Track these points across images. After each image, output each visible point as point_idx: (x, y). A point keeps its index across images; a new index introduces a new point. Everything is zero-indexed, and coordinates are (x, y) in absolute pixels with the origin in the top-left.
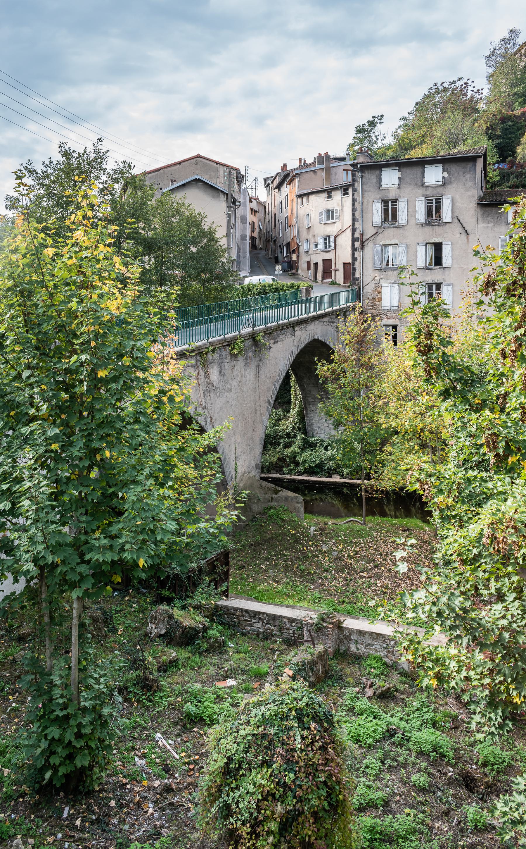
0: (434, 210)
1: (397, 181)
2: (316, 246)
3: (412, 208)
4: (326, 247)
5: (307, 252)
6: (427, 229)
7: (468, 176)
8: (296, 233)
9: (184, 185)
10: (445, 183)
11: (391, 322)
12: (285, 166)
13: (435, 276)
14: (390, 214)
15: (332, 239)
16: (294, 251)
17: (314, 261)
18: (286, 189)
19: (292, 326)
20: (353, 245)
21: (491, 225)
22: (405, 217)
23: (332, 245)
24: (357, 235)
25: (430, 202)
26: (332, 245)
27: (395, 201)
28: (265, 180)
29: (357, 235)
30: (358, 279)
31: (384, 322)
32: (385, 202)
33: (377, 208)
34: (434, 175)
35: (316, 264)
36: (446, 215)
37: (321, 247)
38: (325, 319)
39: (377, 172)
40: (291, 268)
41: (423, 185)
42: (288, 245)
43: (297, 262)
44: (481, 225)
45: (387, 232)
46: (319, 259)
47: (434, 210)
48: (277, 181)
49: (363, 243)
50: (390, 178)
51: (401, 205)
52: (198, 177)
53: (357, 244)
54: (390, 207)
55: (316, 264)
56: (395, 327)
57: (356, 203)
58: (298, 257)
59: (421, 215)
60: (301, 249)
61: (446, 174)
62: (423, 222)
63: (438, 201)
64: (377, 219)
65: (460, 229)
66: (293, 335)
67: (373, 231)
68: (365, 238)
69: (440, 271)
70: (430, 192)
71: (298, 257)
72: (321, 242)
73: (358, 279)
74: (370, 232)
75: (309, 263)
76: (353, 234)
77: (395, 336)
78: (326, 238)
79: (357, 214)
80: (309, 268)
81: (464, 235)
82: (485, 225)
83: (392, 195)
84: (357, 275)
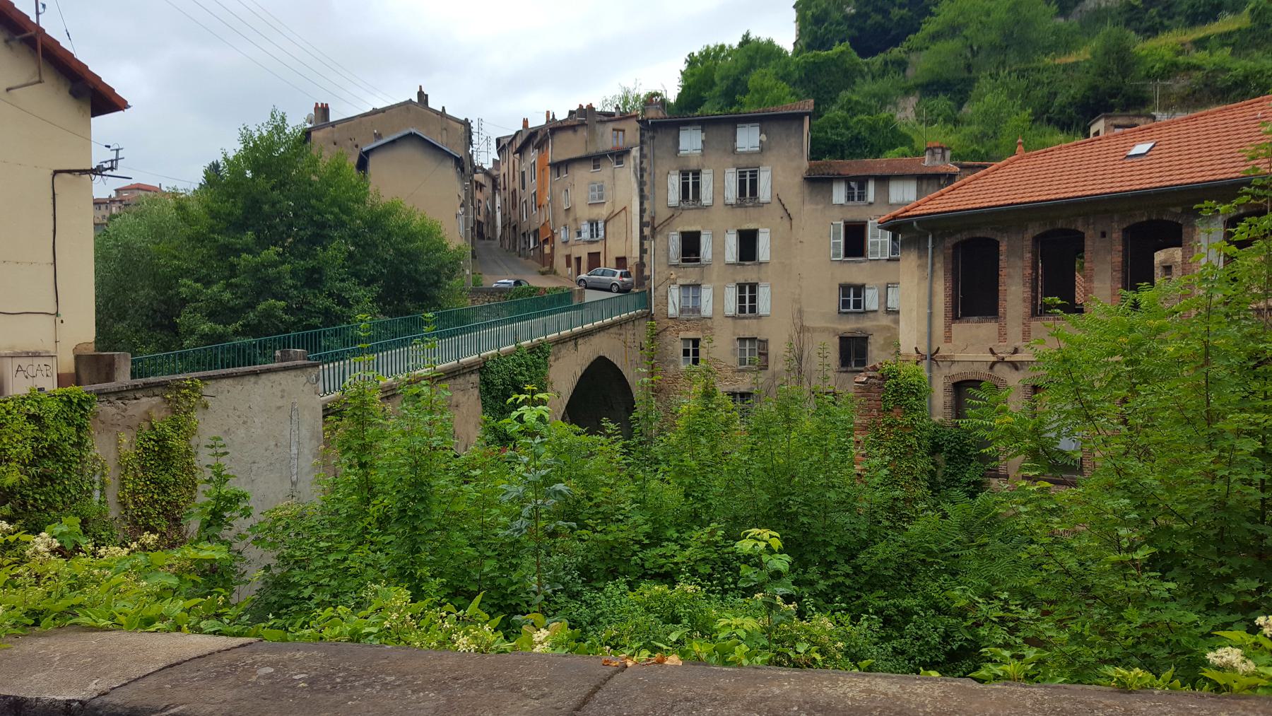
0: (748, 187)
1: (700, 146)
2: (579, 234)
3: (720, 184)
4: (592, 236)
5: (566, 242)
6: (739, 211)
7: (792, 140)
8: (550, 216)
9: (393, 142)
10: (763, 148)
11: (692, 335)
12: (526, 122)
13: (748, 274)
14: (690, 190)
15: (601, 225)
16: (546, 241)
17: (575, 254)
18: (533, 155)
19: (575, 337)
20: (641, 231)
21: (820, 207)
22: (710, 195)
23: (602, 233)
24: (646, 219)
25: (742, 175)
26: (602, 233)
27: (697, 173)
28: (498, 140)
29: (646, 219)
30: (649, 278)
31: (682, 335)
32: (684, 174)
33: (674, 181)
34: (748, 138)
35: (579, 259)
36: (764, 192)
37: (586, 235)
38: (612, 330)
39: (674, 132)
40: (547, 265)
41: (734, 150)
42: (536, 232)
43: (552, 255)
44: (808, 207)
45: (686, 213)
46: (583, 252)
47: (748, 187)
48: (518, 143)
49: (654, 229)
50: (691, 141)
51: (706, 180)
52: (413, 131)
53: (647, 231)
54: (691, 181)
55: (579, 259)
56: (696, 342)
57: (645, 175)
58: (552, 249)
59: (731, 193)
60: (557, 238)
61: (764, 138)
62: (733, 201)
63: (754, 175)
64: (674, 196)
65: (782, 212)
66: (576, 350)
67: (667, 213)
68: (657, 223)
69: (756, 268)
70: (743, 162)
71: (552, 249)
72: (585, 228)
73: (649, 278)
74: (663, 214)
75: (568, 257)
76: (641, 217)
77: (696, 353)
78: (593, 223)
79: (646, 189)
80: (569, 264)
81: (786, 219)
82: (814, 207)
83: (693, 165)
84: (646, 273)
